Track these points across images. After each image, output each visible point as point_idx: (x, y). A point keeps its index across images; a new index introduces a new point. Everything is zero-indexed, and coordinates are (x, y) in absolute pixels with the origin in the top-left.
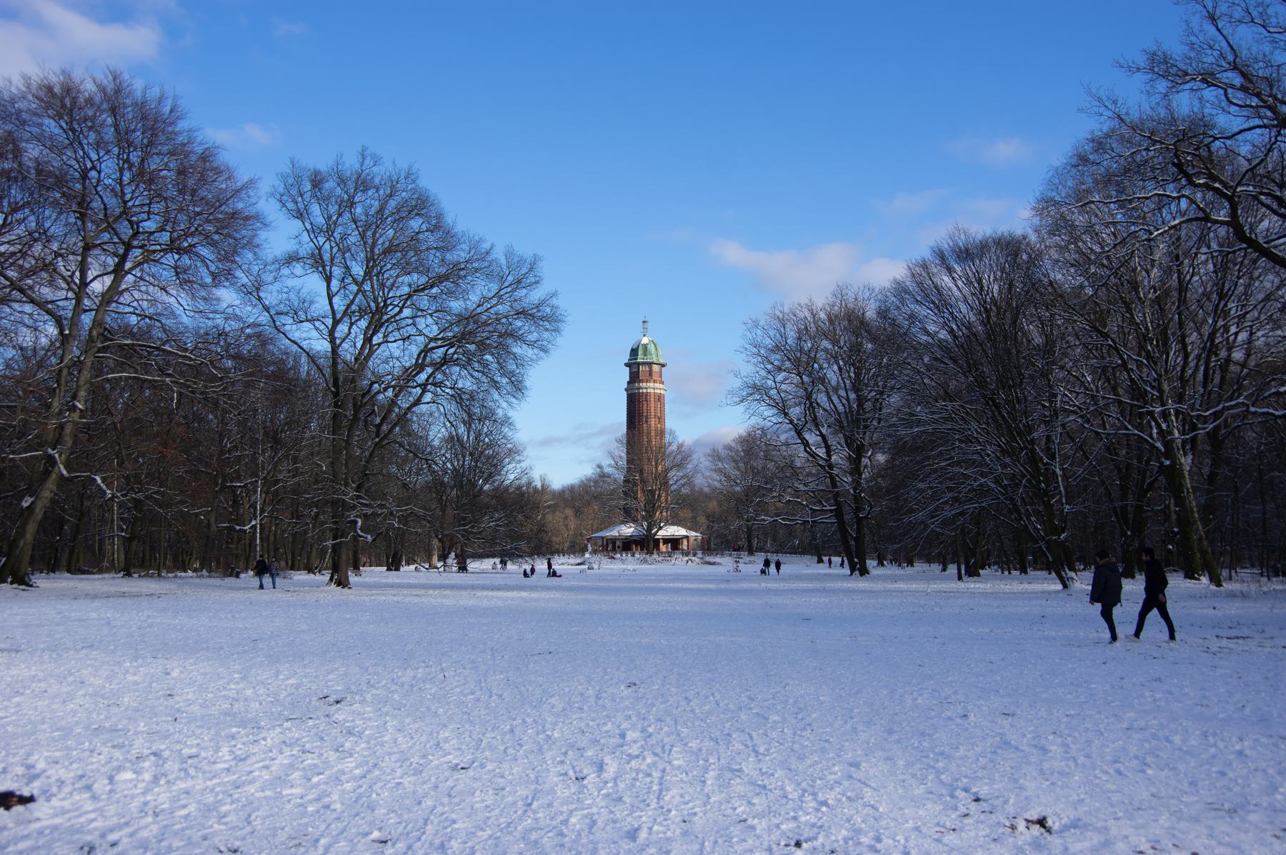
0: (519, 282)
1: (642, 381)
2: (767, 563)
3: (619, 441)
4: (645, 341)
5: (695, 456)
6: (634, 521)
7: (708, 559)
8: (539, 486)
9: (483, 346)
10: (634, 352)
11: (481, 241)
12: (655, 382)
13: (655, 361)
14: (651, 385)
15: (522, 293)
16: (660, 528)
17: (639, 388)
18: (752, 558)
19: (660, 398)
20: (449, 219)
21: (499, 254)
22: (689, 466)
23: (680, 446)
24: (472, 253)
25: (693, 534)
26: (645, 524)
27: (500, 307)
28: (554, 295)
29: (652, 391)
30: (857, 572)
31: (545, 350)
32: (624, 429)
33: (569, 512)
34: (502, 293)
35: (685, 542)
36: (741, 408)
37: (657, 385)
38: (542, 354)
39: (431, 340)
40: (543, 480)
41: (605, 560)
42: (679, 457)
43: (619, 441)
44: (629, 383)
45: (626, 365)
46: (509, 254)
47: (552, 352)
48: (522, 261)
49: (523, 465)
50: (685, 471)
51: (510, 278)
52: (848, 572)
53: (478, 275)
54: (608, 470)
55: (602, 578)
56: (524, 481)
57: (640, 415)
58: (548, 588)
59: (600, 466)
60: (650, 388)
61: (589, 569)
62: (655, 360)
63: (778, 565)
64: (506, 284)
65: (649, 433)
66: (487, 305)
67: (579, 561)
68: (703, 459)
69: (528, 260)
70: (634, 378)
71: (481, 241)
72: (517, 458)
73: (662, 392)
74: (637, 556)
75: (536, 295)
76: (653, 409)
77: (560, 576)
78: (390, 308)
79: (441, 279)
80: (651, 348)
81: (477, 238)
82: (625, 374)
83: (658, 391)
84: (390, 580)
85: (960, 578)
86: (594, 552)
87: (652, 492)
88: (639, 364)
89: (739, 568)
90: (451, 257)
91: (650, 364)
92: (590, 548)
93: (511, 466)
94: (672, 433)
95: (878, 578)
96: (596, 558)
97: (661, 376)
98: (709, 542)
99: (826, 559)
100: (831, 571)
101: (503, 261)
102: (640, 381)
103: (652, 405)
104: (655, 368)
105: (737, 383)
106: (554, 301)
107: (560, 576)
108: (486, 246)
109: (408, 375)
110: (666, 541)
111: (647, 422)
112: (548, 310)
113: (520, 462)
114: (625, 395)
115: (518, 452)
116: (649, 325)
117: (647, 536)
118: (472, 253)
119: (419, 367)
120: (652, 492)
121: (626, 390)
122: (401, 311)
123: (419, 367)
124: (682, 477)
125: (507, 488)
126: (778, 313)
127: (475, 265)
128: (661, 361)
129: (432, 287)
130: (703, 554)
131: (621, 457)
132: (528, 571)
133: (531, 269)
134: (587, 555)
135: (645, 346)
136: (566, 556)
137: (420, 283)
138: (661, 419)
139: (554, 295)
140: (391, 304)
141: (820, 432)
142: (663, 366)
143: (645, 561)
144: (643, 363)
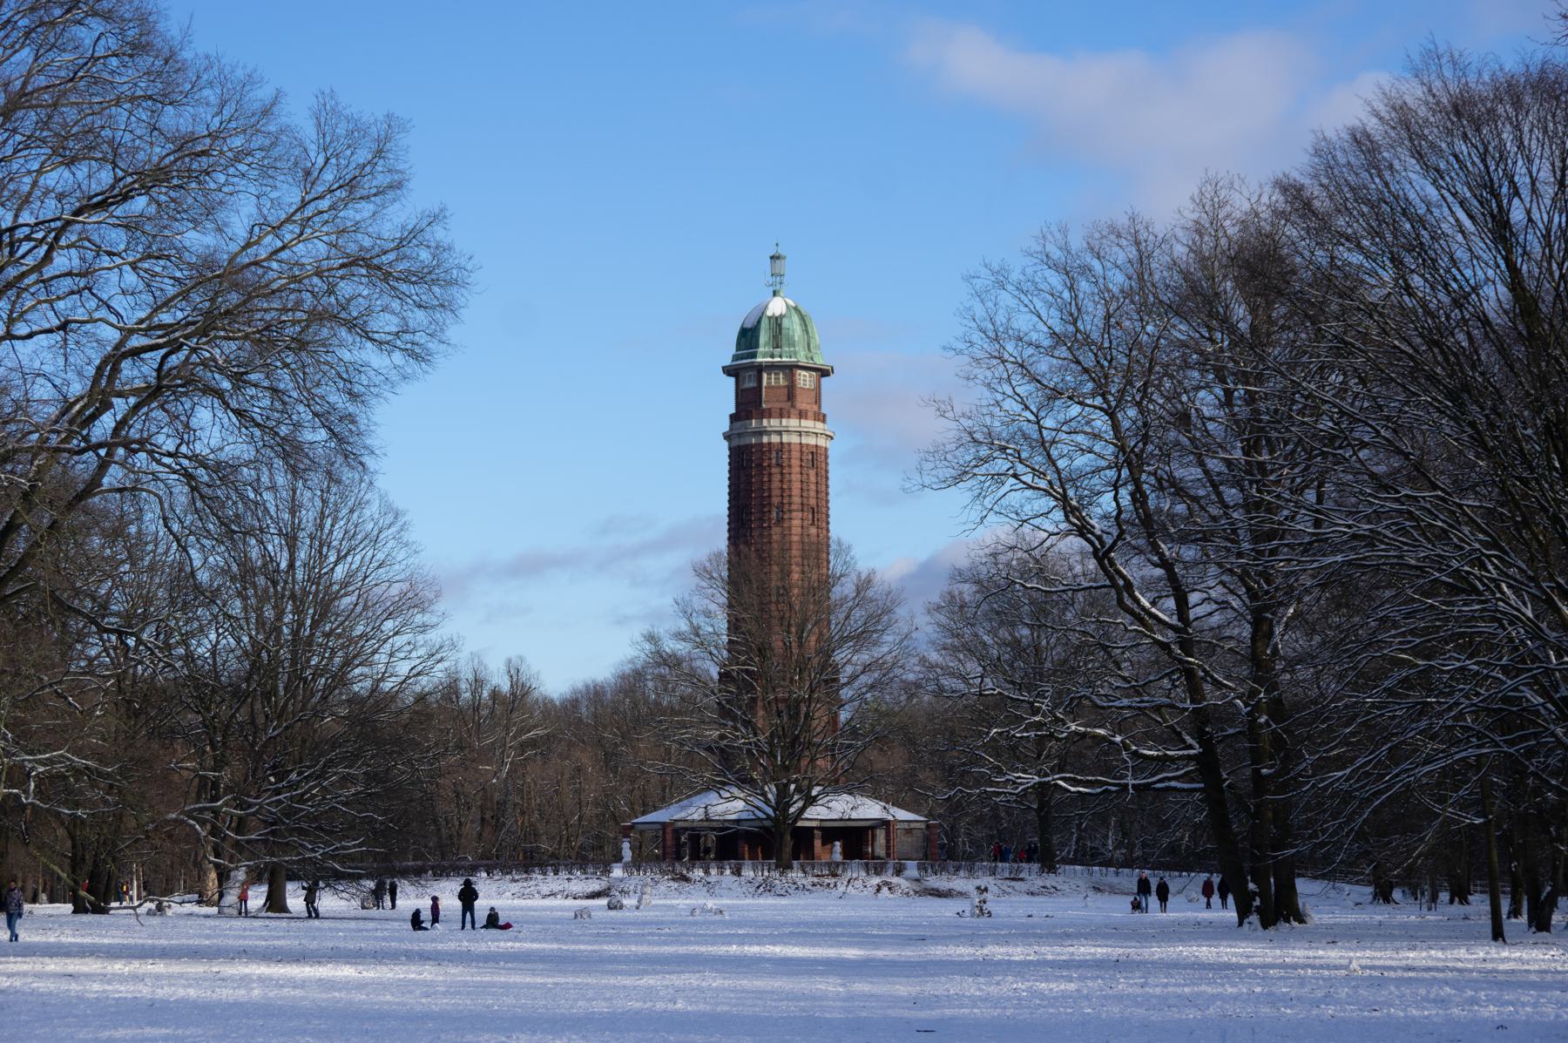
0: (351, 185)
1: (769, 414)
2: (1144, 887)
3: (702, 572)
4: (777, 307)
5: (901, 612)
6: (744, 781)
7: (934, 881)
8: (505, 687)
9: (265, 341)
10: (748, 337)
11: (250, 81)
12: (802, 415)
13: (803, 360)
14: (793, 423)
15: (359, 212)
16: (811, 801)
17: (761, 433)
18: (1050, 880)
19: (816, 459)
20: (170, 27)
21: (298, 116)
22: (888, 638)
23: (864, 585)
24: (226, 113)
25: (902, 815)
26: (771, 791)
27: (300, 248)
28: (435, 218)
29: (795, 439)
30: (1254, 918)
31: (417, 355)
32: (721, 542)
33: (584, 757)
34: (308, 212)
35: (881, 835)
36: (961, 495)
37: (808, 424)
38: (412, 366)
39: (128, 332)
40: (514, 673)
41: (666, 884)
42: (858, 614)
43: (702, 572)
44: (734, 418)
45: (728, 371)
46: (325, 115)
47: (438, 360)
48: (357, 132)
49: (433, 636)
50: (878, 652)
51: (329, 176)
52: (1232, 915)
53: (243, 168)
54: (671, 646)
55: (654, 929)
56: (439, 674)
57: (765, 503)
58: (410, 957)
59: (651, 638)
60: (789, 431)
61: (610, 907)
62: (802, 359)
63: (1163, 893)
64: (320, 189)
65: (786, 548)
66: (272, 243)
67: (595, 886)
68: (922, 620)
69: (373, 130)
70: (748, 405)
71: (250, 81)
72: (419, 619)
73: (822, 442)
74: (748, 873)
75: (393, 220)
76: (796, 486)
77: (507, 926)
78: (25, 247)
79: (152, 178)
80: (793, 326)
81: (240, 73)
82: (724, 395)
83: (812, 441)
84: (493, 947)
85: (1498, 934)
86: (637, 864)
87: (793, 707)
88: (760, 369)
89: (987, 907)
90: (172, 119)
91: (790, 369)
92: (627, 854)
93: (399, 641)
94: (844, 549)
95: (1332, 936)
96: (636, 879)
97: (818, 400)
98: (952, 833)
99: (295, 900)
100: (1171, 915)
101: (308, 131)
102: (763, 414)
103: (796, 477)
104: (804, 379)
105: (944, 431)
106: (439, 234)
107: (507, 926)
108: (263, 94)
109: (77, 415)
110: (831, 833)
111: (780, 521)
112: (425, 255)
113: (424, 628)
114: (723, 449)
115: (421, 605)
116: (787, 267)
117: (775, 820)
118: (226, 113)
119: (99, 400)
120: (793, 707)
121: (727, 437)
122: (47, 258)
123: (99, 400)
124: (866, 668)
125: (392, 697)
126: (1056, 254)
127: (237, 142)
128: (820, 361)
129: (126, 197)
130: (921, 868)
131: (708, 614)
132: (426, 915)
133: (379, 153)
134: (617, 872)
135: (777, 322)
136: (563, 875)
137: (95, 188)
138: (818, 513)
139: (435, 218)
140: (28, 238)
141: (1161, 555)
142: (824, 373)
143: (767, 888)
144: (772, 367)
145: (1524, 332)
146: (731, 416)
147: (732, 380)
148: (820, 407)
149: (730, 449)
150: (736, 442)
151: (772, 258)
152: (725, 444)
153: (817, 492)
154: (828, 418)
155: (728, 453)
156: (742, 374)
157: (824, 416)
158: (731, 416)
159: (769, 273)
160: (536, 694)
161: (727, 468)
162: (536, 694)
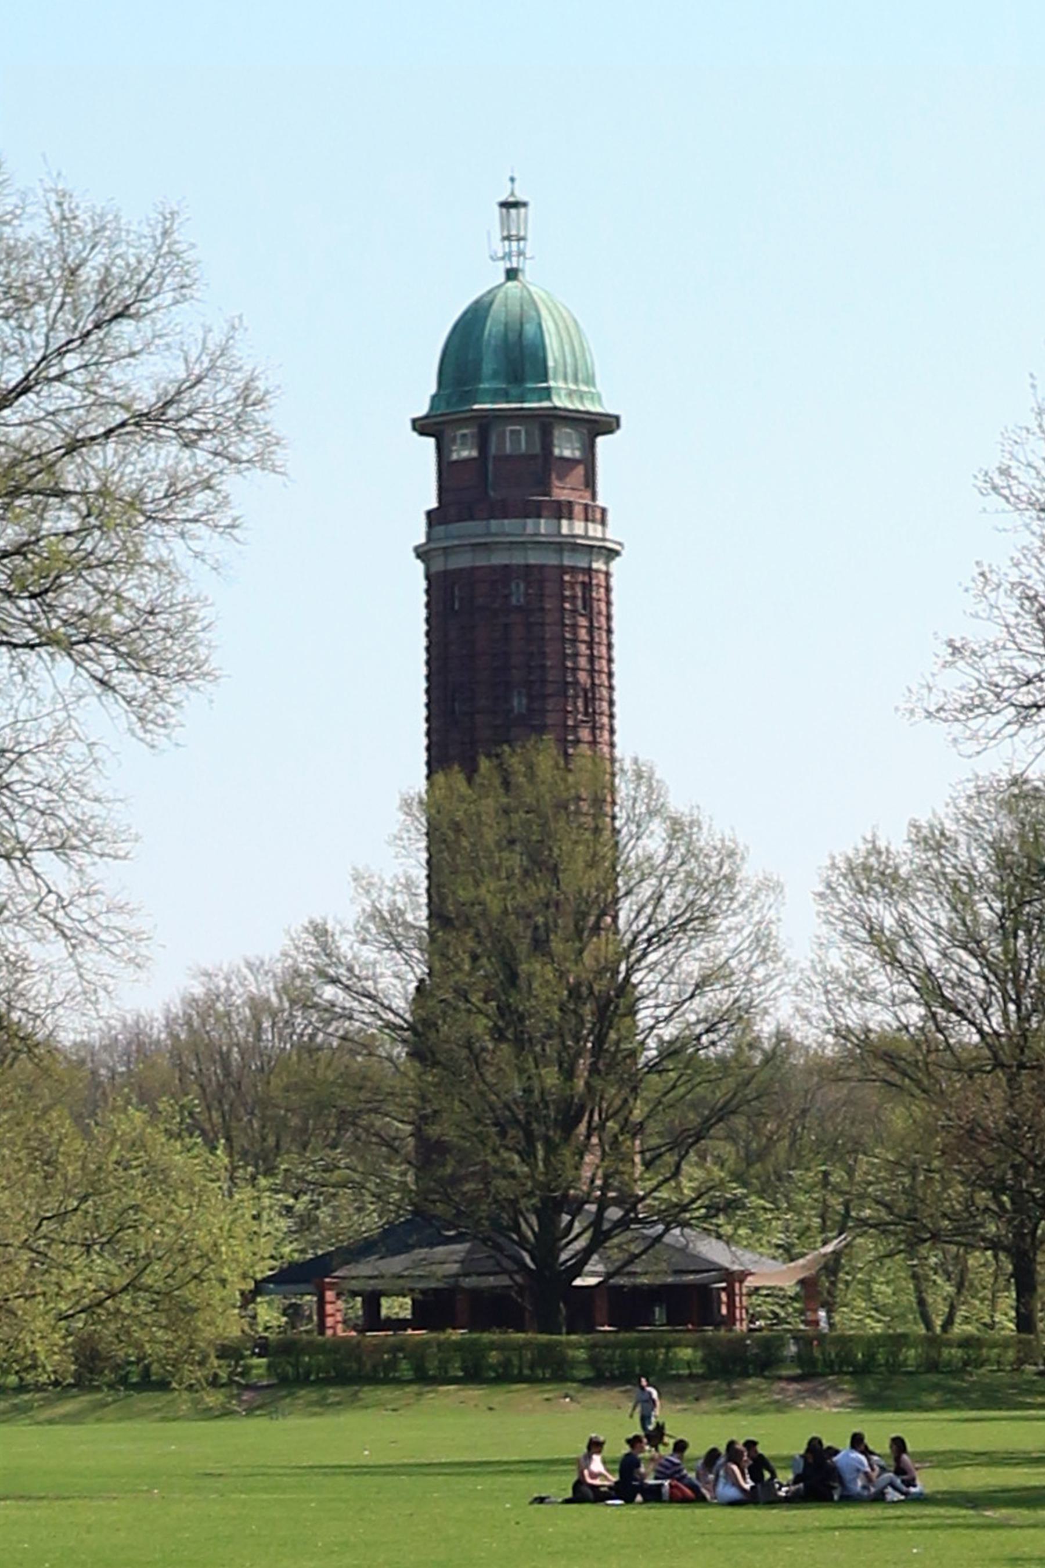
45: (422, 427)
104: (566, 448)
116: (532, 219)
121: (421, 553)
145: (572, 1113)
146: (429, 514)
147: (431, 442)
148: (594, 497)
149: (428, 577)
150: (438, 566)
151: (506, 205)
152: (419, 567)
153: (592, 659)
154: (610, 517)
155: (423, 584)
156: (449, 433)
157: (604, 511)
158: (429, 514)
159: (497, 234)
160: (158, 1032)
161: (423, 642)
162: (158, 1032)
